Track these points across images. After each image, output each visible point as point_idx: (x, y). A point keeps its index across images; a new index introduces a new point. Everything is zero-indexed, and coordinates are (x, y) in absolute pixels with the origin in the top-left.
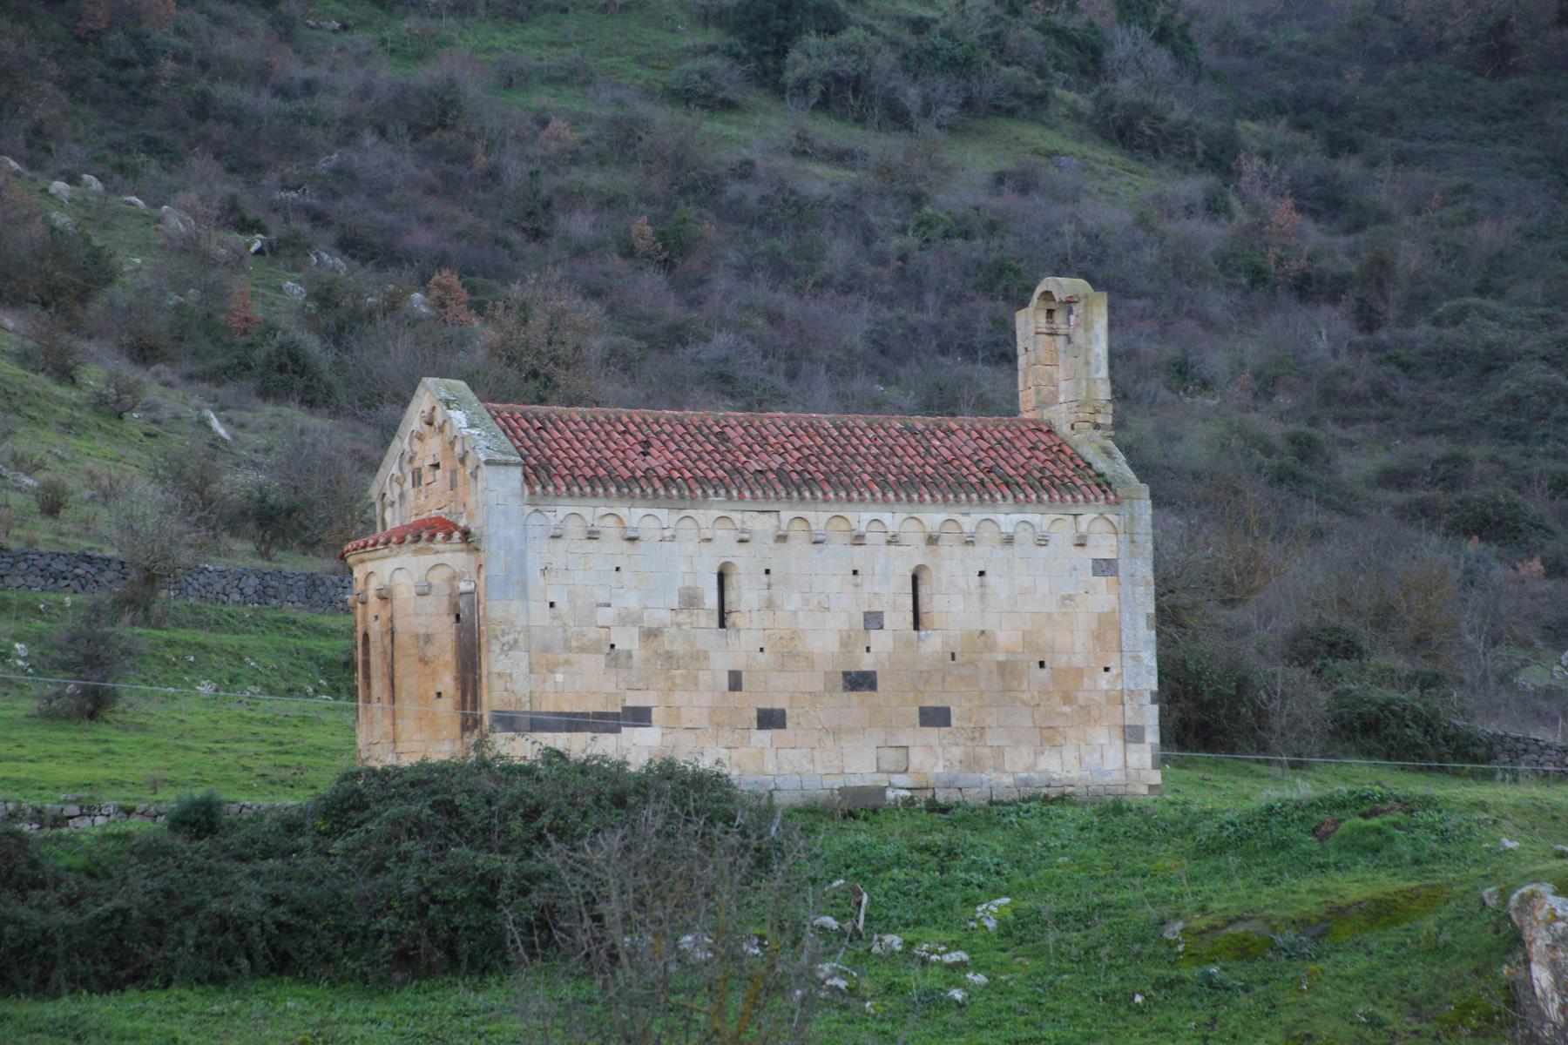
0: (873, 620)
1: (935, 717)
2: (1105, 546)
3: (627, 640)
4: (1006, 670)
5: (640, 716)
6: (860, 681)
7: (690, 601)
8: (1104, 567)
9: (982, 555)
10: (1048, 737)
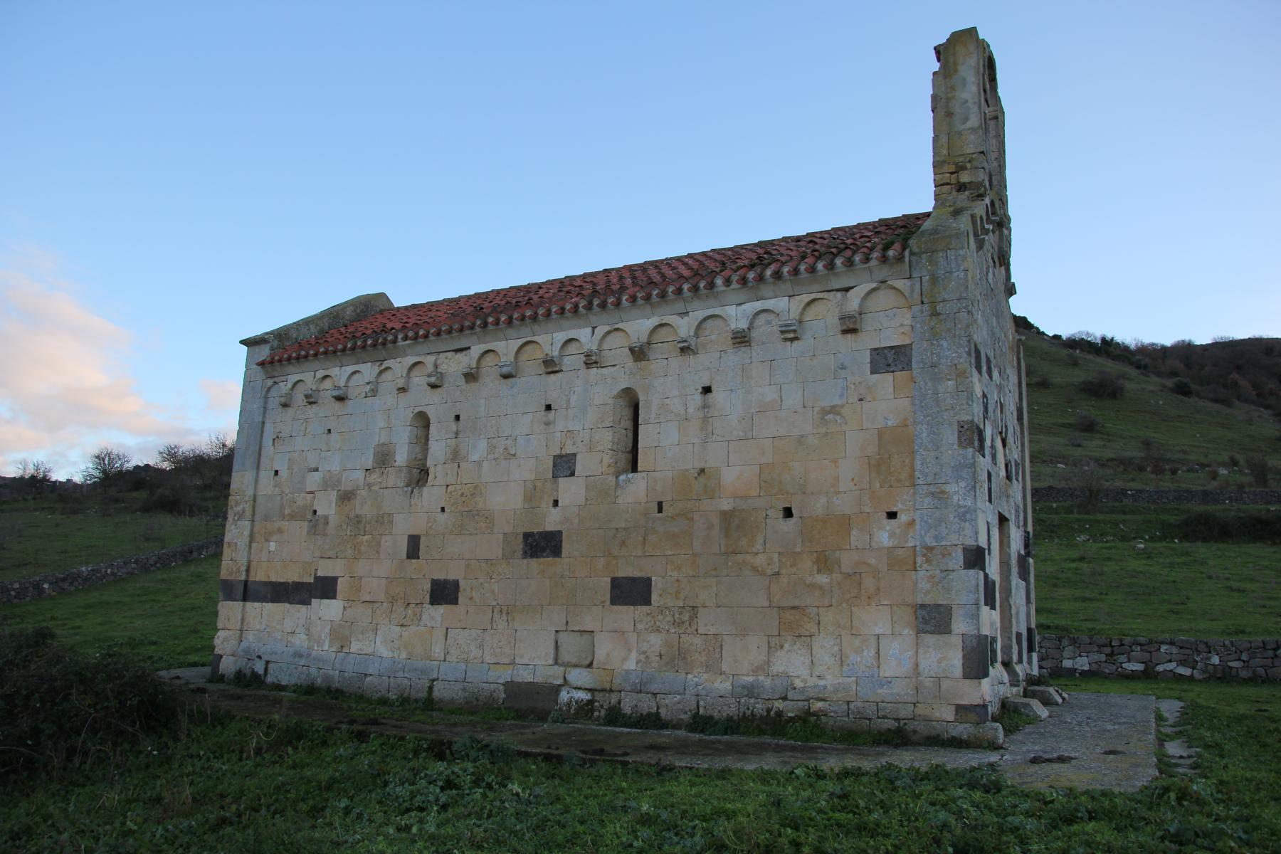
0: (564, 465)
1: (631, 592)
3: (327, 506)
4: (734, 524)
5: (325, 588)
6: (542, 545)
7: (384, 458)
8: (889, 359)
9: (698, 369)
10: (791, 623)
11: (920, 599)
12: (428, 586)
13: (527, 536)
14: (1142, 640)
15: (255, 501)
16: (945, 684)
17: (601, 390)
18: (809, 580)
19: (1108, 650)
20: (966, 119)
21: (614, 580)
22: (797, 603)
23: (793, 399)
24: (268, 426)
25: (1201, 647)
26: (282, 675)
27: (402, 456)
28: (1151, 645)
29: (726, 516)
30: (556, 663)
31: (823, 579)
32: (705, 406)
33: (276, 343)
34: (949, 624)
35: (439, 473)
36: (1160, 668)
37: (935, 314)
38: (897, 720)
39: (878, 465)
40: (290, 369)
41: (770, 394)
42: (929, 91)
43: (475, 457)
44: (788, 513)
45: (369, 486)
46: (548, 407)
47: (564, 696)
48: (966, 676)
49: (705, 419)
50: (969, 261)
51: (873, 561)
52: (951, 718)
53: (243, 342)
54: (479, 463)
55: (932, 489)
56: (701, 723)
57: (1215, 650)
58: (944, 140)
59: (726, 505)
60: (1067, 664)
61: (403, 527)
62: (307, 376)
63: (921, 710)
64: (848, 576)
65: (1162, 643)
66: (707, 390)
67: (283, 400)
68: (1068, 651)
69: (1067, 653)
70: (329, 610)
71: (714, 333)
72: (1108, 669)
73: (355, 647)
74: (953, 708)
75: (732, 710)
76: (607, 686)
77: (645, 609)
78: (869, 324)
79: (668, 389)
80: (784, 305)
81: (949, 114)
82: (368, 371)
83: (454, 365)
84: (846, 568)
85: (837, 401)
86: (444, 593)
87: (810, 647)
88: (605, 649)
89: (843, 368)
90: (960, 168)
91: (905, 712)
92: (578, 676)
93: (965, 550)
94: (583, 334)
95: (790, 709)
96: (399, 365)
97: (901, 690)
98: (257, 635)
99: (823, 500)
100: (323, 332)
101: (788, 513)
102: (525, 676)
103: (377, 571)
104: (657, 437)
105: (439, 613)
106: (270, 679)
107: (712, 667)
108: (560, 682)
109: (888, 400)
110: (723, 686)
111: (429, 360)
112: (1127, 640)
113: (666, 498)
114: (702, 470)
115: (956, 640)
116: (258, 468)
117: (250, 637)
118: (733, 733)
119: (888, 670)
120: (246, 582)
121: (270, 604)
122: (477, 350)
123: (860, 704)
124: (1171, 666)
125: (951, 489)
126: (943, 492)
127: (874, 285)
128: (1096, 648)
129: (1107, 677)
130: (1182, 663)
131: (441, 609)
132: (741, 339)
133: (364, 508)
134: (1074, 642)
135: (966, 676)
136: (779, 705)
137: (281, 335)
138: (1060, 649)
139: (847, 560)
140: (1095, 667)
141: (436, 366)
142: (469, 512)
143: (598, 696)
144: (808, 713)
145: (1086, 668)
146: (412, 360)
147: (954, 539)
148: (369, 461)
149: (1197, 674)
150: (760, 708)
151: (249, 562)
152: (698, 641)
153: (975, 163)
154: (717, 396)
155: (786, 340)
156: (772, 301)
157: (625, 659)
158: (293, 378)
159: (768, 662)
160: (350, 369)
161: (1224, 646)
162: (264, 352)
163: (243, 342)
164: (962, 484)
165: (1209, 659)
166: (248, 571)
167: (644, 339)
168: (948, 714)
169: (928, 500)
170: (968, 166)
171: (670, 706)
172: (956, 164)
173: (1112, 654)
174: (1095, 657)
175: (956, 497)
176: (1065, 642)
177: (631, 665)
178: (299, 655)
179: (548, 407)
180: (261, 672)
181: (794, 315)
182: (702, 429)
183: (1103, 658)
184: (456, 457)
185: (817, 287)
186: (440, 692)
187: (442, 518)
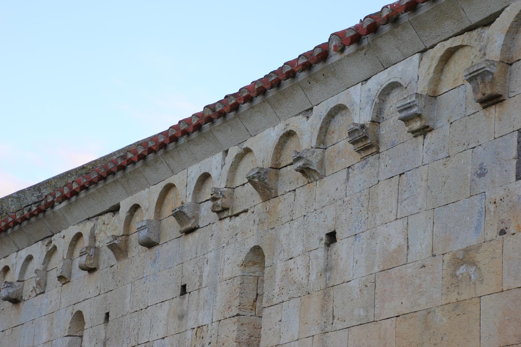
23: (420, 249)
32: (328, 268)
38: (192, 140)
41: (393, 234)
49: (327, 291)
66: (332, 237)
67: (144, 234)
79: (295, 255)
80: (412, 71)
82: (38, 251)
83: (112, 227)
85: (473, 240)
89: (481, 173)
111: (86, 229)
122: (125, 207)
132: (365, 141)
141: (93, 237)
146: (71, 231)
154: (341, 246)
155: (416, 133)
156: (400, 66)
160: (24, 254)
167: (268, 164)
181: (423, 87)
182: (323, 308)
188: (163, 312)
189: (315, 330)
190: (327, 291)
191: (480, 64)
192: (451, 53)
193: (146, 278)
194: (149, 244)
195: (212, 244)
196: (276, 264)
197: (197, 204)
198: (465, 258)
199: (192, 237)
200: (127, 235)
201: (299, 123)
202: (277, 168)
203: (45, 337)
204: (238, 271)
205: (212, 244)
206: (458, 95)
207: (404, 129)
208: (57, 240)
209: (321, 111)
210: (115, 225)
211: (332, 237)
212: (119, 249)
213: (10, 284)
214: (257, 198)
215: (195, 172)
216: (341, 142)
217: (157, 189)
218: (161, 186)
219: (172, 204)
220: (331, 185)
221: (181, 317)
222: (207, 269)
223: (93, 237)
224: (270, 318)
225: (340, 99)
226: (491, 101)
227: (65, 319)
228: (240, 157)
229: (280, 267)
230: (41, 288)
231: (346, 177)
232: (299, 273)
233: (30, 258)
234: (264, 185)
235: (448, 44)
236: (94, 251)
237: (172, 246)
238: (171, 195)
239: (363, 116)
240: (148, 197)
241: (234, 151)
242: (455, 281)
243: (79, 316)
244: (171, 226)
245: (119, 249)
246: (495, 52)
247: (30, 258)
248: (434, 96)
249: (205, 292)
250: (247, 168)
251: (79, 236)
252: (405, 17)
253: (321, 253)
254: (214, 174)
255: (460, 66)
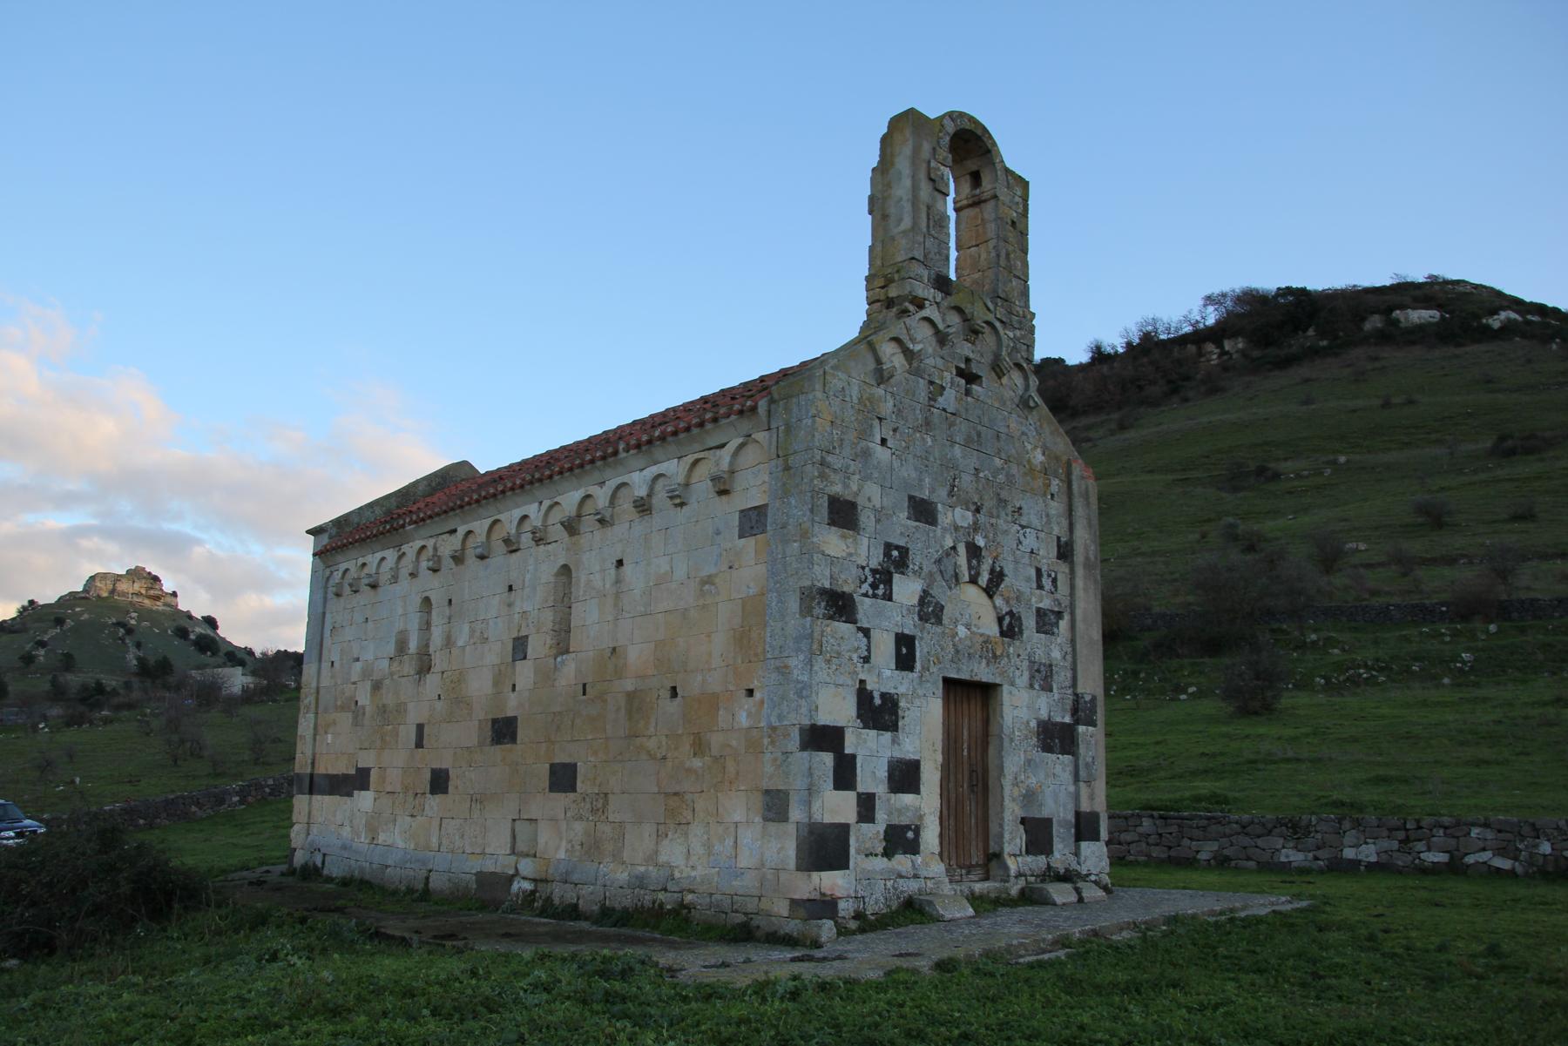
1: (563, 778)
2: (753, 489)
6: (504, 730)
8: (753, 522)
10: (674, 812)
11: (766, 784)
12: (428, 776)
13: (495, 721)
14: (1446, 820)
15: (318, 692)
16: (783, 876)
17: (538, 567)
18: (688, 764)
19: (1401, 835)
20: (900, 220)
21: (552, 765)
22: (677, 789)
23: (681, 572)
24: (328, 616)
25: (1526, 830)
26: (334, 869)
27: (413, 646)
28: (1457, 828)
29: (631, 696)
30: (513, 852)
31: (697, 763)
32: (618, 581)
33: (334, 531)
34: (786, 811)
35: (439, 662)
36: (1470, 859)
37: (787, 468)
38: (746, 914)
39: (742, 639)
40: (339, 558)
41: (664, 566)
42: (867, 191)
43: (460, 643)
44: (674, 692)
45: (392, 674)
46: (511, 588)
47: (515, 887)
48: (798, 869)
49: (617, 595)
50: (820, 414)
51: (734, 743)
52: (786, 914)
53: (308, 532)
54: (463, 648)
55: (778, 663)
56: (607, 915)
57: (1546, 835)
58: (879, 249)
59: (629, 685)
60: (1349, 853)
61: (414, 716)
62: (378, 560)
63: (765, 905)
64: (716, 759)
65: (1474, 824)
66: (620, 563)
67: (479, 551)
68: (1350, 838)
69: (1348, 839)
70: (365, 800)
71: (625, 505)
72: (1401, 860)
73: (381, 838)
74: (787, 903)
75: (627, 902)
76: (543, 876)
77: (572, 795)
78: (740, 482)
79: (593, 569)
80: (673, 468)
81: (885, 217)
82: (391, 555)
83: (449, 545)
84: (715, 752)
85: (713, 571)
86: (439, 783)
87: (686, 834)
88: (545, 836)
89: (718, 533)
90: (889, 282)
91: (751, 906)
92: (527, 867)
93: (801, 730)
94: (532, 510)
95: (668, 900)
96: (410, 549)
97: (747, 883)
98: (330, 829)
99: (699, 678)
100: (389, 512)
101: (674, 692)
102: (489, 866)
103: (395, 764)
104: (589, 617)
105: (434, 803)
106: (325, 872)
107: (617, 857)
108: (511, 872)
109: (749, 568)
110: (622, 876)
111: (430, 543)
112: (1427, 821)
113: (589, 680)
114: (614, 649)
115: (791, 828)
116: (320, 661)
117: (314, 830)
118: (624, 925)
119: (743, 862)
120: (312, 776)
121: (327, 798)
122: (462, 530)
123: (719, 897)
124: (1485, 856)
125: (793, 662)
126: (786, 667)
127: (741, 440)
128: (1385, 833)
129: (1399, 872)
130: (1501, 852)
131: (438, 798)
132: (643, 507)
133: (389, 699)
134: (1357, 824)
135: (798, 869)
136: (661, 896)
137: (341, 523)
138: (1340, 833)
139: (716, 740)
140: (1384, 857)
141: (435, 549)
142: (456, 699)
143: (541, 886)
144: (682, 905)
145: (1373, 859)
146: (418, 544)
147: (792, 718)
148: (391, 649)
149: (1519, 869)
150: (647, 900)
151: (314, 755)
152: (607, 829)
153: (903, 274)
154: (627, 569)
155: (676, 505)
156: (665, 465)
157: (558, 848)
158: (343, 567)
159: (656, 852)
160: (379, 555)
161: (1558, 828)
162: (325, 539)
163: (308, 532)
164: (801, 657)
165: (1536, 846)
166: (313, 763)
167: (573, 513)
168: (782, 908)
169: (774, 676)
170: (896, 277)
171: (588, 896)
172: (885, 276)
173: (1406, 841)
174: (1385, 844)
175: (795, 672)
176: (1347, 825)
177: (562, 855)
178: (344, 847)
179: (511, 588)
180: (319, 864)
181: (681, 479)
182: (616, 605)
183: (1395, 845)
184: (449, 642)
185: (697, 446)
186: (436, 882)
187: (439, 705)
188: (495, 601)
189: (610, 618)
190: (617, 595)
191: (714, 470)
192: (697, 461)
193: (481, 585)
194: (482, 557)
195: (531, 561)
196: (581, 577)
197: (519, 534)
198: (709, 580)
199: (514, 555)
200: (463, 549)
201: (594, 490)
202: (579, 516)
203: (400, 611)
204: (552, 579)
205: (531, 561)
206: (702, 486)
207: (669, 502)
208: (405, 548)
209: (612, 484)
210: (454, 542)
211: (620, 563)
212: (458, 559)
213: (369, 576)
214: (565, 534)
215: (517, 513)
216: (625, 505)
217: (487, 523)
218: (490, 521)
219: (499, 534)
220: (619, 530)
221: (510, 605)
222: (528, 576)
223: (435, 549)
224: (577, 609)
225: (625, 479)
226: (723, 492)
227: (417, 601)
228: (551, 507)
229: (583, 579)
230: (395, 579)
231: (628, 529)
232: (598, 583)
233: (383, 559)
234: (571, 527)
235: (697, 456)
236: (437, 558)
237: (499, 558)
238: (497, 527)
239: (642, 492)
240: (480, 526)
241: (547, 503)
242: (702, 594)
243: (427, 600)
244: (499, 547)
245: (458, 559)
246: (725, 464)
247: (383, 559)
248: (687, 485)
249: (527, 590)
250: (557, 516)
251: (424, 547)
252: (670, 439)
253: (613, 571)
254: (532, 516)
255: (703, 471)
